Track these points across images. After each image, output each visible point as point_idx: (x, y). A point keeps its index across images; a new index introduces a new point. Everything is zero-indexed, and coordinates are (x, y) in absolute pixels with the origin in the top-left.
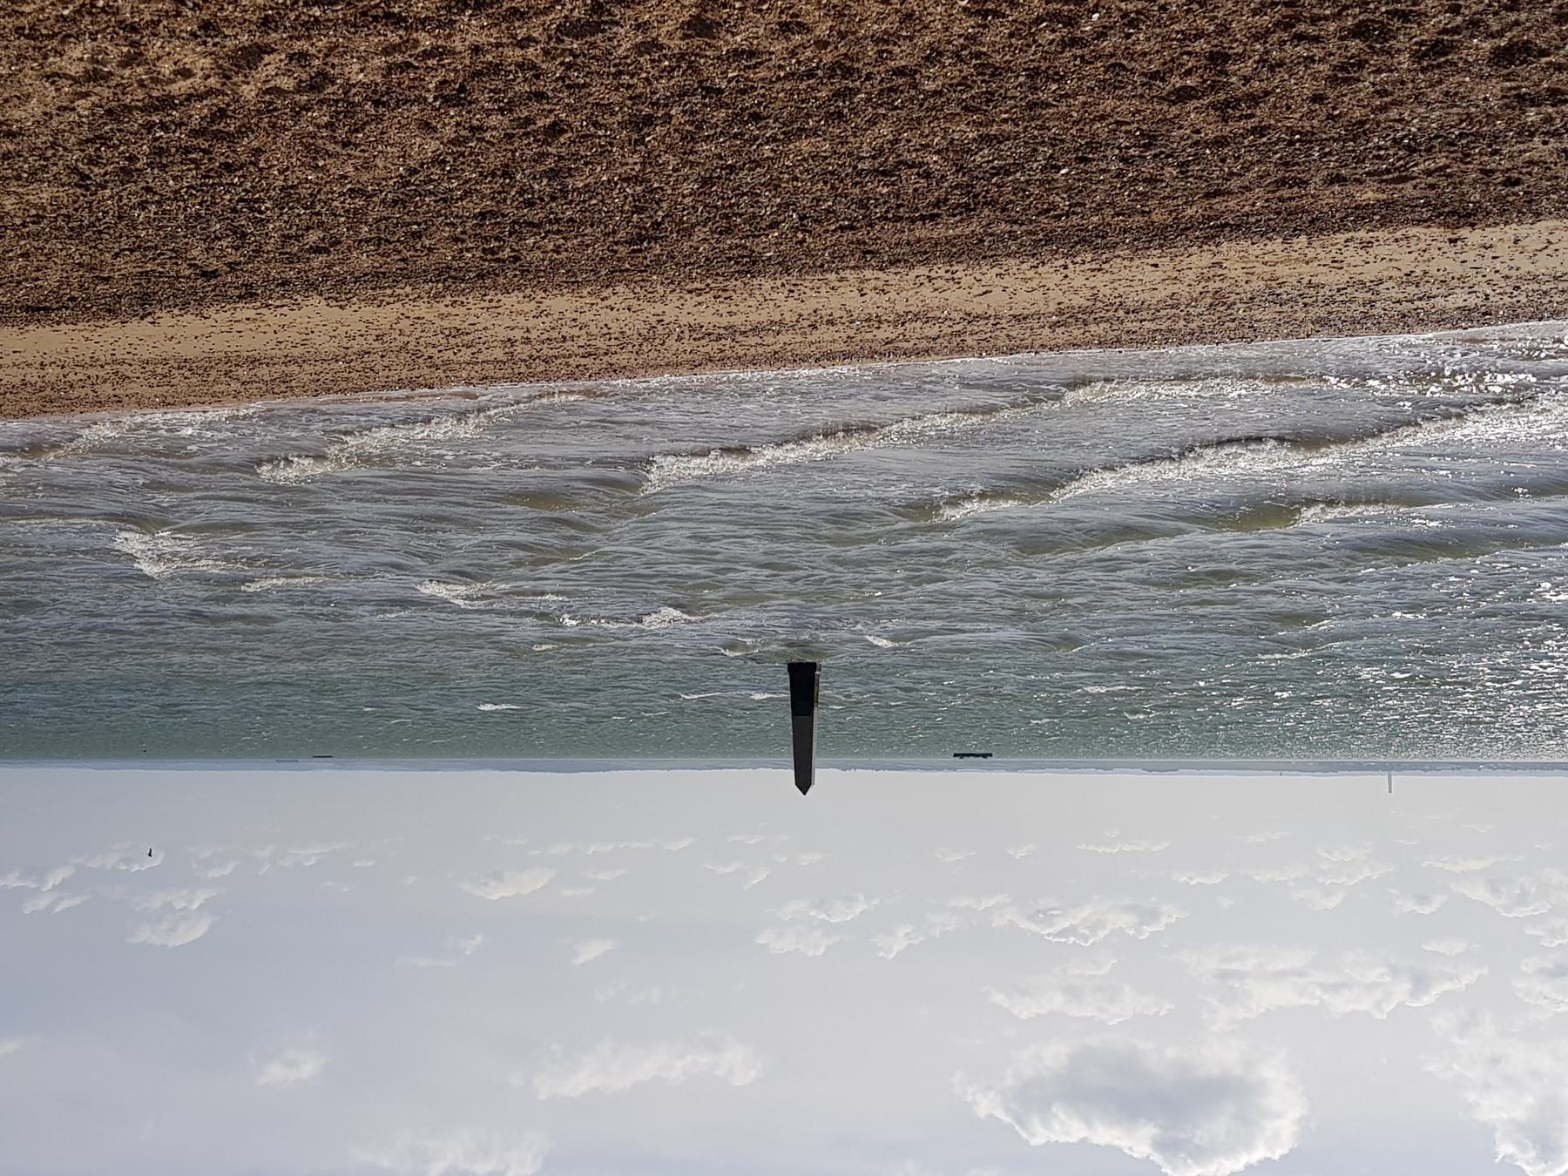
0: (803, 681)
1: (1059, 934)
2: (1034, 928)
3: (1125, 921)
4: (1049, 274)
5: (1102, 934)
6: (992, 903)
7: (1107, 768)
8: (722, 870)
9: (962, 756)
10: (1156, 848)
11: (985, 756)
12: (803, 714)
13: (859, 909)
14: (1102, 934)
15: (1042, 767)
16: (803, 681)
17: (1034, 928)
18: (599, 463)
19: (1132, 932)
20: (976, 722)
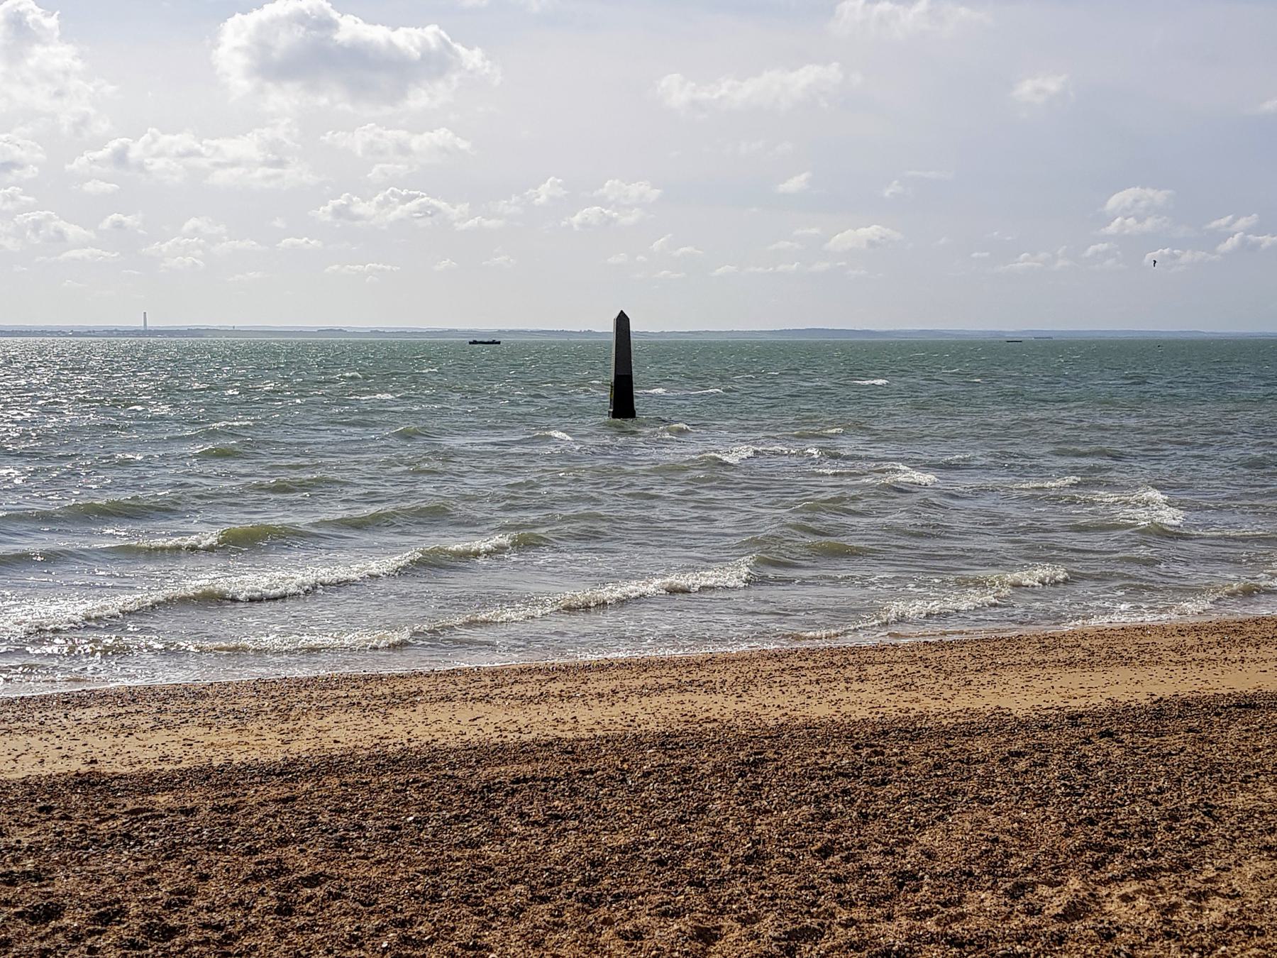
1: (417, 196)
2: (435, 202)
3: (361, 208)
6: (470, 222)
7: (375, 332)
9: (493, 342)
10: (336, 267)
11: (475, 342)
12: (622, 377)
14: (380, 197)
17: (435, 202)
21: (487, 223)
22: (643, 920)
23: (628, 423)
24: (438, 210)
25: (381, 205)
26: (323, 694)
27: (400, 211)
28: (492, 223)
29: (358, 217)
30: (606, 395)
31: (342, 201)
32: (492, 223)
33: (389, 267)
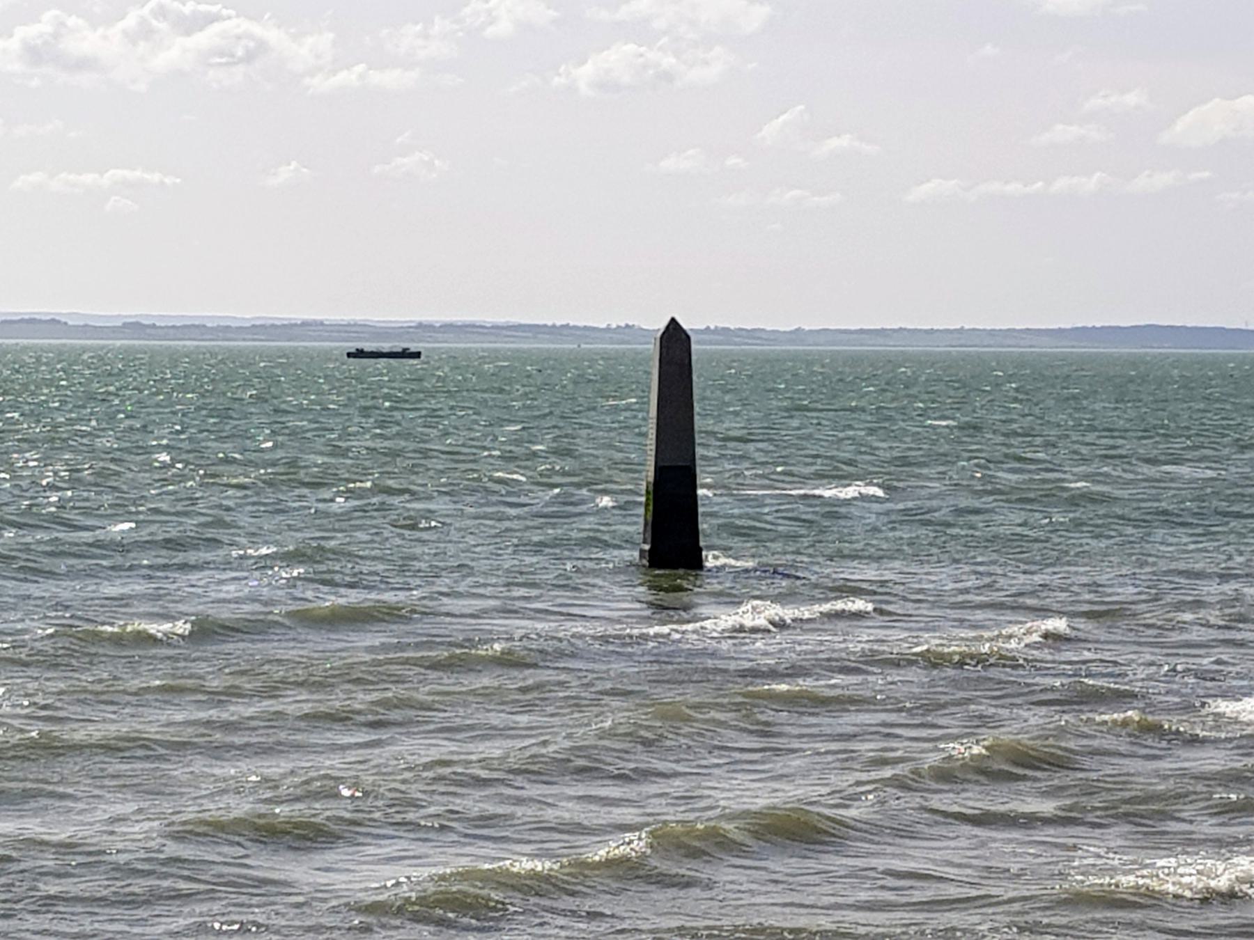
0: (673, 541)
1: (215, 18)
2: (257, 29)
3: (86, 41)
4: (850, 677)
5: (131, 21)
6: (342, 77)
7: (135, 328)
8: (844, 141)
9: (405, 354)
10: (36, 177)
11: (359, 354)
12: (673, 452)
13: (588, 70)
14: (131, 21)
15: (258, 329)
16: (673, 541)
17: (257, 29)
18: (1178, 654)
19: (72, 21)
20: (358, 421)
21: (376, 77)
22: (607, 472)
23: (681, 577)
24: (262, 47)
25: (131, 38)
26: (949, 910)
27: (177, 51)
28: (389, 78)
29: (83, 64)
30: (635, 525)
31: (44, 27)
32: (389, 78)
33: (156, 177)
